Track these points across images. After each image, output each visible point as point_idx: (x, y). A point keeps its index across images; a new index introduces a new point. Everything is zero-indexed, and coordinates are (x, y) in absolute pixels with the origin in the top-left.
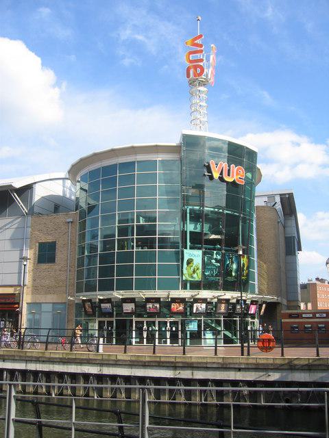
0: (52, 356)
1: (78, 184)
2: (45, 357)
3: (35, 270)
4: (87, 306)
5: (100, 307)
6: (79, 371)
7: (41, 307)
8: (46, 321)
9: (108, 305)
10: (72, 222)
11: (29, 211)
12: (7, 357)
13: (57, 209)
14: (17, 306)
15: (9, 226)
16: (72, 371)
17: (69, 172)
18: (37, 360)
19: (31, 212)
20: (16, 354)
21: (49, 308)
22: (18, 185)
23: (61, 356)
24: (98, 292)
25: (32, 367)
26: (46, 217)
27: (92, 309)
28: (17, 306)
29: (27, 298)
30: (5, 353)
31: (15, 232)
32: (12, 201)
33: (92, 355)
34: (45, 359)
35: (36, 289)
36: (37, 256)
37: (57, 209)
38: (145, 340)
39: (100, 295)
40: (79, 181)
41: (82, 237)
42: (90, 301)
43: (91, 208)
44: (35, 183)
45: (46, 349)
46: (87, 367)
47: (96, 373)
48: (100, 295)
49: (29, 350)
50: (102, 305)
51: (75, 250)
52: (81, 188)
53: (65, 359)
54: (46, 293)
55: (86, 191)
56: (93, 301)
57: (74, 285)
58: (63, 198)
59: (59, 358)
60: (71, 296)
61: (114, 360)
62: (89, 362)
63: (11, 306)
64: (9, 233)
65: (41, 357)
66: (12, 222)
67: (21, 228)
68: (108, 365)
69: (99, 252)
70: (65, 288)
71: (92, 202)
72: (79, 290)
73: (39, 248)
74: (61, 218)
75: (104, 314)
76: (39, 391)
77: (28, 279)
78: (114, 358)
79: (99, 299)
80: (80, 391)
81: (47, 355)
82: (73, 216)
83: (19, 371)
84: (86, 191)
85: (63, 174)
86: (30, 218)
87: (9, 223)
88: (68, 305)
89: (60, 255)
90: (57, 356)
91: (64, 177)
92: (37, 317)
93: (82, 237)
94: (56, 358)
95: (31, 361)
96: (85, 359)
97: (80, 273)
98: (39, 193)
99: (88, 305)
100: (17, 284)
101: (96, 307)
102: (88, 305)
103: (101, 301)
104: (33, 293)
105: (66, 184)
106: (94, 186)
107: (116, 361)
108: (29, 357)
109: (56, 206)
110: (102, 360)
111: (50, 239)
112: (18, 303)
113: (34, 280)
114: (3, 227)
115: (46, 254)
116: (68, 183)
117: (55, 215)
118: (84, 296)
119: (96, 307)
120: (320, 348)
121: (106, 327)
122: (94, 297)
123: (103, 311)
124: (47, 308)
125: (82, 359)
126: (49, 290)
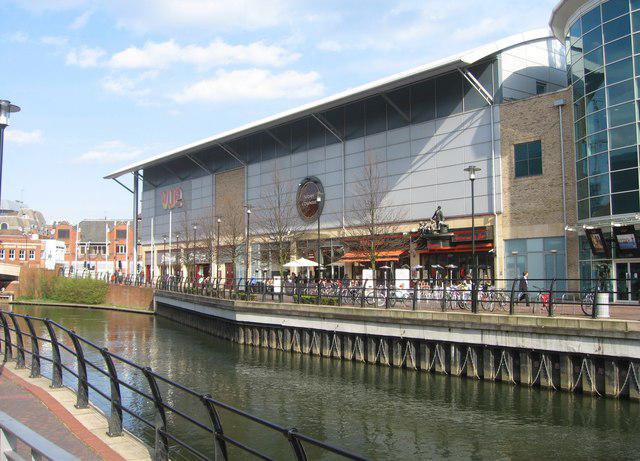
0: (520, 323)
1: (568, 42)
2: (509, 326)
3: (513, 189)
4: (594, 240)
5: (616, 240)
6: (564, 350)
7: (526, 244)
8: (535, 269)
9: (629, 237)
10: (562, 106)
11: (494, 99)
12: (453, 326)
13: (541, 87)
14: (490, 245)
15: (469, 124)
16: (554, 349)
17: (551, 24)
18: (498, 330)
19: (499, 98)
20: (467, 319)
21: (538, 245)
22: (471, 58)
23: (534, 324)
24: (612, 217)
25: (491, 340)
26: (522, 103)
27: (604, 244)
28: (490, 245)
29: (502, 234)
30: (451, 319)
31: (476, 134)
32: (468, 86)
33: (584, 323)
34: (508, 329)
35: (516, 218)
36: (514, 166)
37: (541, 87)
38: (630, 295)
39: (616, 221)
40: (568, 38)
41: (581, 128)
42: (598, 231)
43: (594, 80)
44: (500, 52)
45: (511, 312)
46: (282, 319)
47: (592, 352)
48: (616, 221)
49: (490, 314)
50: (620, 237)
51: (572, 150)
52: (573, 48)
53: (541, 328)
54: (531, 223)
55: (579, 50)
56: (604, 231)
57: (574, 206)
58: (550, 70)
59: (531, 327)
60: (571, 225)
61: (622, 332)
62: (579, 334)
63: (483, 246)
64: (468, 137)
65: (504, 325)
66: (473, 116)
67: (487, 124)
68: (613, 340)
69: (609, 149)
70: (560, 213)
71: (595, 68)
72: (583, 215)
73: (516, 154)
74: (546, 101)
75: (622, 252)
76: (469, 374)
77: (502, 203)
78: (621, 328)
79: (615, 228)
80: (567, 382)
81: (512, 322)
82: (565, 94)
83: (473, 346)
84: (579, 50)
85: (546, 32)
86: (497, 108)
87: (470, 118)
88: (569, 239)
89: (548, 161)
90: (528, 324)
91: (547, 35)
92: (521, 260)
93: (581, 128)
94: (526, 327)
95: (489, 330)
96: (573, 330)
97: (581, 186)
98: (508, 67)
99: (595, 238)
100: (487, 211)
101: (610, 241)
102: (595, 238)
103: (618, 231)
104: (512, 225)
105: (554, 47)
106: (590, 40)
107: (626, 334)
108: (485, 324)
109: (539, 83)
110: (602, 331)
111: (530, 137)
112: (492, 241)
113: (512, 204)
114: (461, 126)
115: (528, 162)
116: (557, 44)
117: (534, 99)
118: (589, 225)
119: (610, 241)
120: (529, 250)
121: (628, 273)
122: (605, 224)
123: (622, 246)
124: (536, 246)
125: (568, 329)
126: (536, 218)
